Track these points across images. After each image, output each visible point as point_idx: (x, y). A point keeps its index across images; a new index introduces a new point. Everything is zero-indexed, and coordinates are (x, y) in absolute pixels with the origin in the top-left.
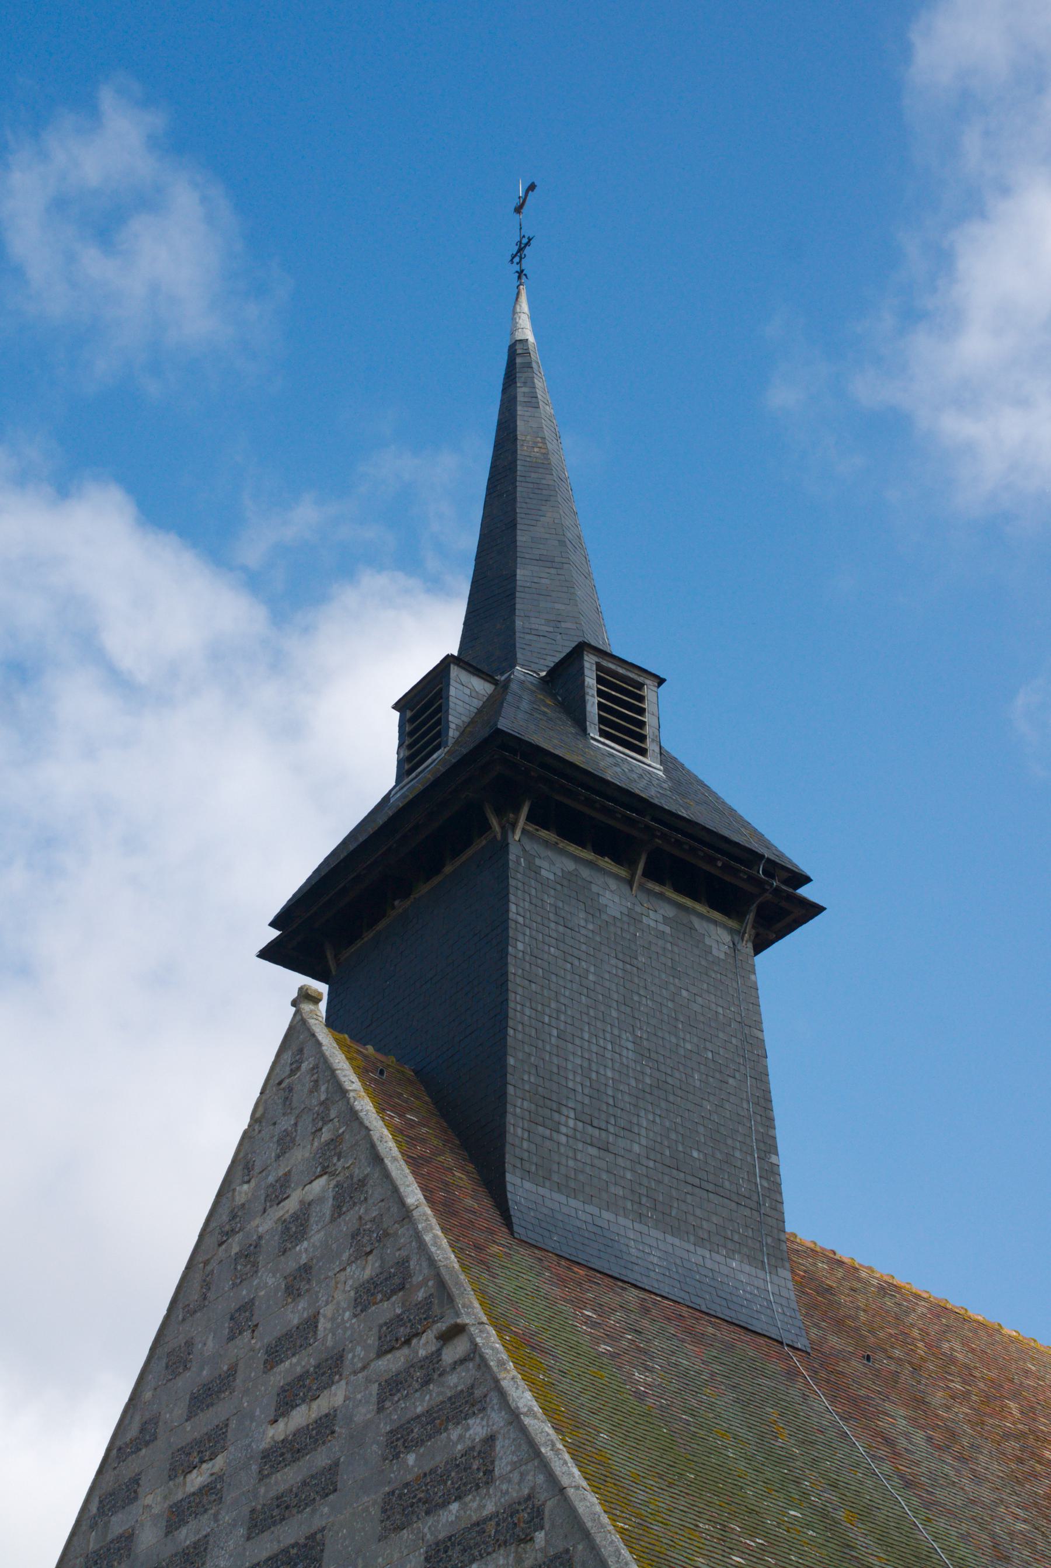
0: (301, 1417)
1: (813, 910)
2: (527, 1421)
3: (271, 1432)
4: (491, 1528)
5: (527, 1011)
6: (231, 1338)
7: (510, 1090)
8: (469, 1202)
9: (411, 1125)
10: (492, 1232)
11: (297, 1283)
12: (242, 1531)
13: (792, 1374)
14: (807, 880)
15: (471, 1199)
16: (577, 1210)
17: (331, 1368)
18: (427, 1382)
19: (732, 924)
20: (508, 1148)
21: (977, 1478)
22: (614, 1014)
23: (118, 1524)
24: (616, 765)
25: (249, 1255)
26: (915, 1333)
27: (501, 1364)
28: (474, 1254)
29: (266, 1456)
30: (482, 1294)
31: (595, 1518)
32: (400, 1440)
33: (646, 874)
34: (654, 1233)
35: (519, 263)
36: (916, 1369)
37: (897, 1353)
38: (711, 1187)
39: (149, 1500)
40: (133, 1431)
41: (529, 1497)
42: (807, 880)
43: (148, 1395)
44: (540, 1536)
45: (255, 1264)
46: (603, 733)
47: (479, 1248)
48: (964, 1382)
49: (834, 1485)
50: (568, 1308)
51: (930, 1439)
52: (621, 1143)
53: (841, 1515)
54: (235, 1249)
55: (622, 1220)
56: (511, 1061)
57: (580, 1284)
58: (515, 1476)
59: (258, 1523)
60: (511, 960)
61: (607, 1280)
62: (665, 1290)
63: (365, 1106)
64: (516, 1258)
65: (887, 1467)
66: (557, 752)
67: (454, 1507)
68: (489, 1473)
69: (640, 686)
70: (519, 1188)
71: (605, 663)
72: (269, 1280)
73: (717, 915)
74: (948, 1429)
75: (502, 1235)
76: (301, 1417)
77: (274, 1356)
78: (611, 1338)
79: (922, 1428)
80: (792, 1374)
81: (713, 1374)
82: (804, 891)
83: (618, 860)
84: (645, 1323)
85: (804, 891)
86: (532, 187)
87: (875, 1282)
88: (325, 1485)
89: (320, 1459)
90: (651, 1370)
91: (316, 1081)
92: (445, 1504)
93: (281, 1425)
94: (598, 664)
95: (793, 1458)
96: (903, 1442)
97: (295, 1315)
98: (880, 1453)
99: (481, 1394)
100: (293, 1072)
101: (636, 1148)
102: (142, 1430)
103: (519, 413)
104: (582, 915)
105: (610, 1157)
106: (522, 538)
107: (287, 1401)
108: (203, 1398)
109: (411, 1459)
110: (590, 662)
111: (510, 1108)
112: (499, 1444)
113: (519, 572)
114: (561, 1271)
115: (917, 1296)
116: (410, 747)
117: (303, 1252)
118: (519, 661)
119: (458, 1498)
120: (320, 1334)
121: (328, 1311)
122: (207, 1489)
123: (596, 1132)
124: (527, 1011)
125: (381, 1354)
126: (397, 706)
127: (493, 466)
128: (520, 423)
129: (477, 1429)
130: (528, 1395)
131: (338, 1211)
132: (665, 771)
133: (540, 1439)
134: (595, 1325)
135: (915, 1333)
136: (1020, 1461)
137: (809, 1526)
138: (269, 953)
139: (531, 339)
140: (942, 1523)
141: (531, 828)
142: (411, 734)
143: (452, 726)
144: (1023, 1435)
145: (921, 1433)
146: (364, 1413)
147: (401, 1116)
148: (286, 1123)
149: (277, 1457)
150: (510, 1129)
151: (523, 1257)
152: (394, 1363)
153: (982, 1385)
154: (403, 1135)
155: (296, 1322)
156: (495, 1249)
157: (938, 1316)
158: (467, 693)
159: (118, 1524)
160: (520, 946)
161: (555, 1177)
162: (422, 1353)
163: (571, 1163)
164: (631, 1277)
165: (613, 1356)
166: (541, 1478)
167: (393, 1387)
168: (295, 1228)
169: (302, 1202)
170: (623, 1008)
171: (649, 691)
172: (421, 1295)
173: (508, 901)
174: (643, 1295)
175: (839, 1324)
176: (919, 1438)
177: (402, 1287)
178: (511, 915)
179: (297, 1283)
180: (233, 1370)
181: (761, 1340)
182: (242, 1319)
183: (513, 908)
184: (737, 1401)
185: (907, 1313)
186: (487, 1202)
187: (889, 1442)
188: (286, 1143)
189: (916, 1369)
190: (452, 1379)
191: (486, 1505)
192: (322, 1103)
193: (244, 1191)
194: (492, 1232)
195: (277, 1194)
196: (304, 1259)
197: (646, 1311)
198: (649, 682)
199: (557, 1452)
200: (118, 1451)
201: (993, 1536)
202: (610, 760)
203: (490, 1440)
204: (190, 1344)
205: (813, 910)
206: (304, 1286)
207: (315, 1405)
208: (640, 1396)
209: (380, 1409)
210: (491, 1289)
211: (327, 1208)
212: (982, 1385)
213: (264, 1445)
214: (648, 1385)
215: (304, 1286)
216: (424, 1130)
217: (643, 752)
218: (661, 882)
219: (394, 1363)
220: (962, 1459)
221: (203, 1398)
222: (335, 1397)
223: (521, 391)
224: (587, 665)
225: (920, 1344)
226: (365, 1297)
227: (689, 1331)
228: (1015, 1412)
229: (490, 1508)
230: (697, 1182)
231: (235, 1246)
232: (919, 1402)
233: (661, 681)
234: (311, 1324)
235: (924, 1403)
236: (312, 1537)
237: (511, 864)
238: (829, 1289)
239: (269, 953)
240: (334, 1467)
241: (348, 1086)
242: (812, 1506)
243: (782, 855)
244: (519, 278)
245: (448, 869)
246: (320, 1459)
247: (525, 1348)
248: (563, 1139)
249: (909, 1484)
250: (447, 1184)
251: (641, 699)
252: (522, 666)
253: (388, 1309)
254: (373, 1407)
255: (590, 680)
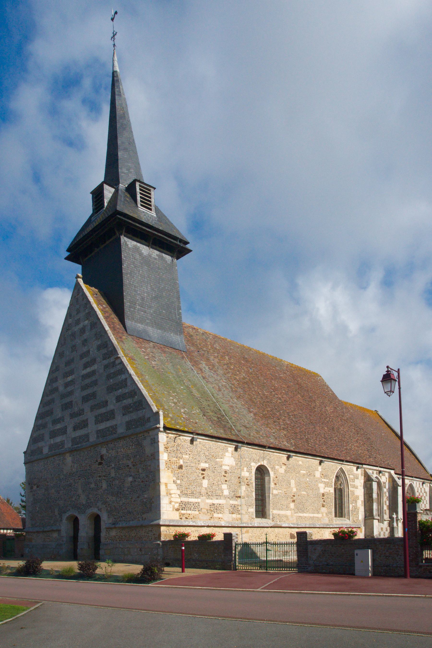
0: (88, 370)
1: (189, 251)
2: (133, 376)
3: (83, 372)
4: (127, 394)
5: (127, 281)
6: (72, 352)
7: (125, 300)
8: (118, 326)
9: (104, 308)
10: (123, 333)
11: (85, 343)
12: (80, 390)
13: (183, 357)
14: (189, 243)
15: (118, 325)
16: (140, 326)
17: (93, 361)
18: (113, 366)
19: (172, 254)
20: (125, 314)
21: (218, 375)
22: (146, 280)
23: (55, 385)
24: (145, 215)
25: (73, 335)
26: (209, 343)
27: (127, 365)
28: (120, 339)
29: (83, 376)
30: (122, 348)
31: (146, 395)
32: (109, 377)
33: (152, 244)
34: (155, 330)
35: (114, 41)
36: (208, 352)
37: (205, 349)
38: (167, 319)
39: (60, 381)
40: (54, 368)
41: (134, 390)
42: (189, 243)
43: (56, 361)
44: (136, 397)
45: (75, 337)
46: (142, 205)
47: (121, 338)
48: (218, 353)
49: (190, 380)
50: (139, 349)
51: (209, 368)
52: (148, 310)
53: (190, 387)
54: (70, 333)
55: (149, 328)
56: (124, 294)
57: (141, 343)
58: (131, 386)
59: (83, 388)
60: (123, 269)
61: (147, 341)
62: (158, 342)
63: (95, 306)
64: (128, 339)
65: (200, 375)
66: (131, 215)
67: (120, 390)
68: (126, 385)
69: (150, 190)
70: (128, 323)
71: (141, 185)
72: (78, 341)
73: (168, 253)
74: (213, 365)
75: (126, 334)
76: (88, 370)
77: (82, 357)
78: (148, 355)
79: (208, 366)
80: (183, 357)
81: (167, 360)
82: (188, 246)
83: (146, 241)
84: (154, 350)
85: (188, 246)
86: (116, 13)
87: (201, 332)
88: (95, 383)
89: (93, 378)
90: (155, 361)
91: (83, 298)
92: (118, 389)
93: (85, 371)
94: (140, 185)
95: (182, 376)
96: (204, 369)
97: (85, 349)
98: (199, 372)
99: (124, 370)
100: (78, 295)
101: (152, 311)
102: (56, 368)
103: (116, 98)
104: (138, 256)
105: (146, 314)
106: (119, 142)
107: (86, 366)
108: (68, 363)
109: (111, 380)
110: (138, 184)
111: (125, 305)
112: (128, 380)
113: (119, 153)
114: (137, 340)
115: (210, 334)
116: (96, 205)
117: (85, 336)
118: (120, 182)
119: (121, 389)
120: (91, 354)
121: (91, 349)
122: (72, 381)
123: (143, 309)
124: (127, 281)
125: (103, 360)
126: (91, 193)
127: (110, 116)
128: (117, 102)
129: (123, 377)
130: (133, 371)
131: (91, 329)
132: (156, 214)
133: (135, 380)
134: (144, 352)
135: (209, 343)
136: (226, 369)
137: (185, 389)
138: (67, 258)
139: (118, 70)
140: (210, 385)
141: (126, 234)
142: (96, 202)
143: (105, 202)
144: (228, 364)
145: (208, 367)
146: (101, 371)
147: (102, 306)
148: (78, 307)
149: (85, 377)
150: (125, 309)
151: (130, 338)
152: (106, 362)
153: (221, 354)
154: (103, 311)
155: (85, 351)
156: (124, 337)
157: (214, 339)
158: (109, 192)
159: (55, 385)
160: (125, 265)
161: (135, 320)
162: (112, 361)
163: (138, 316)
164: (151, 340)
165: (148, 359)
166: (136, 387)
167: (106, 367)
168: (83, 331)
169: (83, 325)
170: (148, 279)
171: (152, 192)
172: (110, 349)
173: (121, 254)
174: (153, 344)
175: (193, 345)
176: (207, 368)
177: (106, 347)
178: (123, 258)
179: (85, 343)
180: (73, 359)
181: (177, 351)
182: (74, 348)
183: (123, 256)
184: (172, 365)
185: (207, 339)
186: (122, 326)
187: (201, 370)
188: (78, 312)
189: (208, 352)
190: (118, 367)
191: (126, 390)
192: (85, 303)
193: (70, 321)
194: (123, 333)
195: (78, 322)
196: (85, 338)
197: (154, 347)
198: (152, 189)
199: (139, 382)
200: (51, 372)
201: (219, 386)
202: (143, 214)
203: (126, 379)
204: (63, 351)
205: (189, 251)
206: (86, 344)
207: (91, 368)
208: (153, 367)
209: (104, 370)
210: (124, 347)
211: (89, 327)
212: (221, 354)
213: (82, 374)
214: (155, 364)
215: (86, 344)
216: (107, 309)
217: (150, 209)
218: (156, 245)
219: (106, 362)
220: (215, 371)
221: (68, 363)
222: (95, 367)
223: (117, 90)
224: (137, 185)
225: (210, 346)
226: (99, 348)
227: (163, 351)
228: (227, 359)
229: (127, 391)
230: (164, 318)
231: (70, 332)
232: (208, 360)
233: (155, 188)
234: (89, 351)
235: (209, 360)
236: (94, 392)
237: (122, 244)
238: (192, 336)
239: (67, 258)
240: (97, 380)
241: (90, 300)
242: (185, 385)
243: (183, 237)
244: (114, 46)
245: (107, 242)
246: (93, 378)
247: (131, 359)
248: (136, 311)
249: (204, 378)
250: (113, 322)
251: (150, 194)
252: (121, 184)
253: (104, 351)
254: (103, 370)
255: (138, 190)
